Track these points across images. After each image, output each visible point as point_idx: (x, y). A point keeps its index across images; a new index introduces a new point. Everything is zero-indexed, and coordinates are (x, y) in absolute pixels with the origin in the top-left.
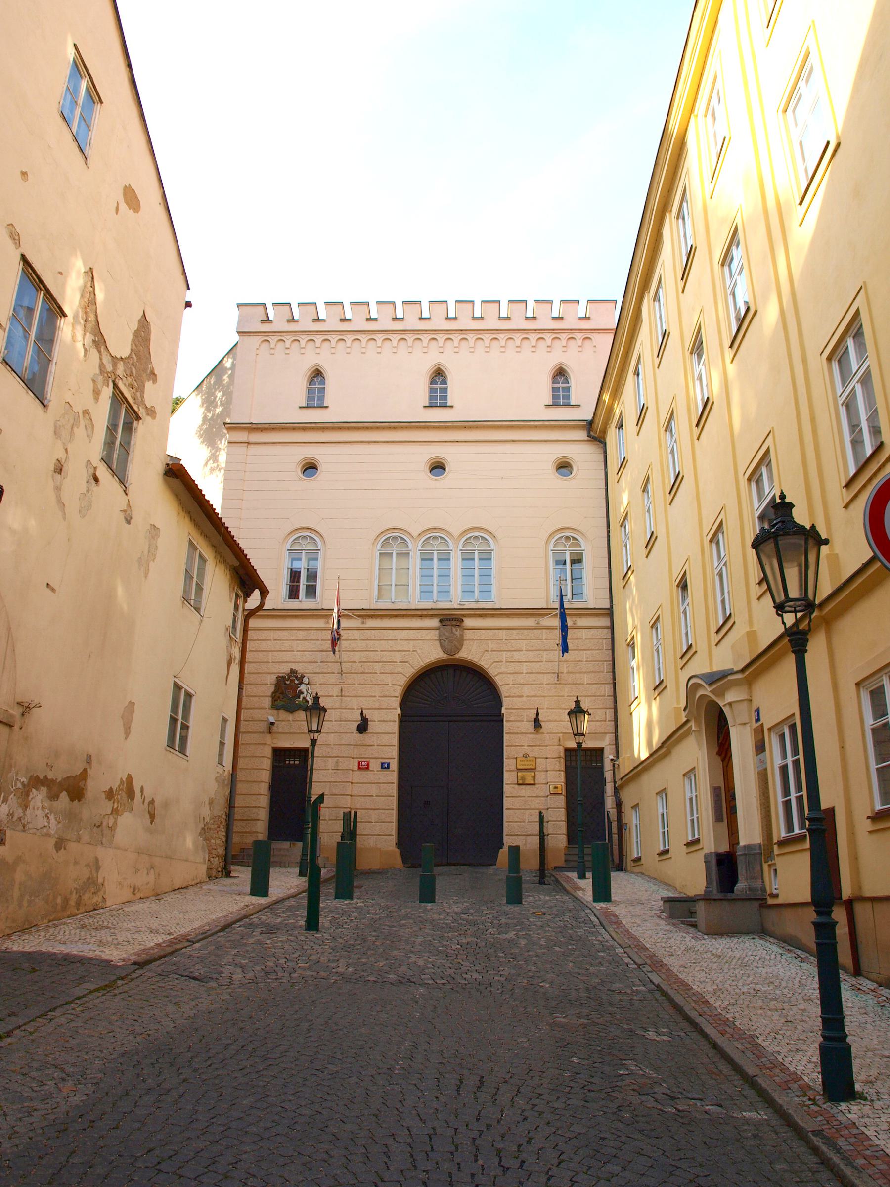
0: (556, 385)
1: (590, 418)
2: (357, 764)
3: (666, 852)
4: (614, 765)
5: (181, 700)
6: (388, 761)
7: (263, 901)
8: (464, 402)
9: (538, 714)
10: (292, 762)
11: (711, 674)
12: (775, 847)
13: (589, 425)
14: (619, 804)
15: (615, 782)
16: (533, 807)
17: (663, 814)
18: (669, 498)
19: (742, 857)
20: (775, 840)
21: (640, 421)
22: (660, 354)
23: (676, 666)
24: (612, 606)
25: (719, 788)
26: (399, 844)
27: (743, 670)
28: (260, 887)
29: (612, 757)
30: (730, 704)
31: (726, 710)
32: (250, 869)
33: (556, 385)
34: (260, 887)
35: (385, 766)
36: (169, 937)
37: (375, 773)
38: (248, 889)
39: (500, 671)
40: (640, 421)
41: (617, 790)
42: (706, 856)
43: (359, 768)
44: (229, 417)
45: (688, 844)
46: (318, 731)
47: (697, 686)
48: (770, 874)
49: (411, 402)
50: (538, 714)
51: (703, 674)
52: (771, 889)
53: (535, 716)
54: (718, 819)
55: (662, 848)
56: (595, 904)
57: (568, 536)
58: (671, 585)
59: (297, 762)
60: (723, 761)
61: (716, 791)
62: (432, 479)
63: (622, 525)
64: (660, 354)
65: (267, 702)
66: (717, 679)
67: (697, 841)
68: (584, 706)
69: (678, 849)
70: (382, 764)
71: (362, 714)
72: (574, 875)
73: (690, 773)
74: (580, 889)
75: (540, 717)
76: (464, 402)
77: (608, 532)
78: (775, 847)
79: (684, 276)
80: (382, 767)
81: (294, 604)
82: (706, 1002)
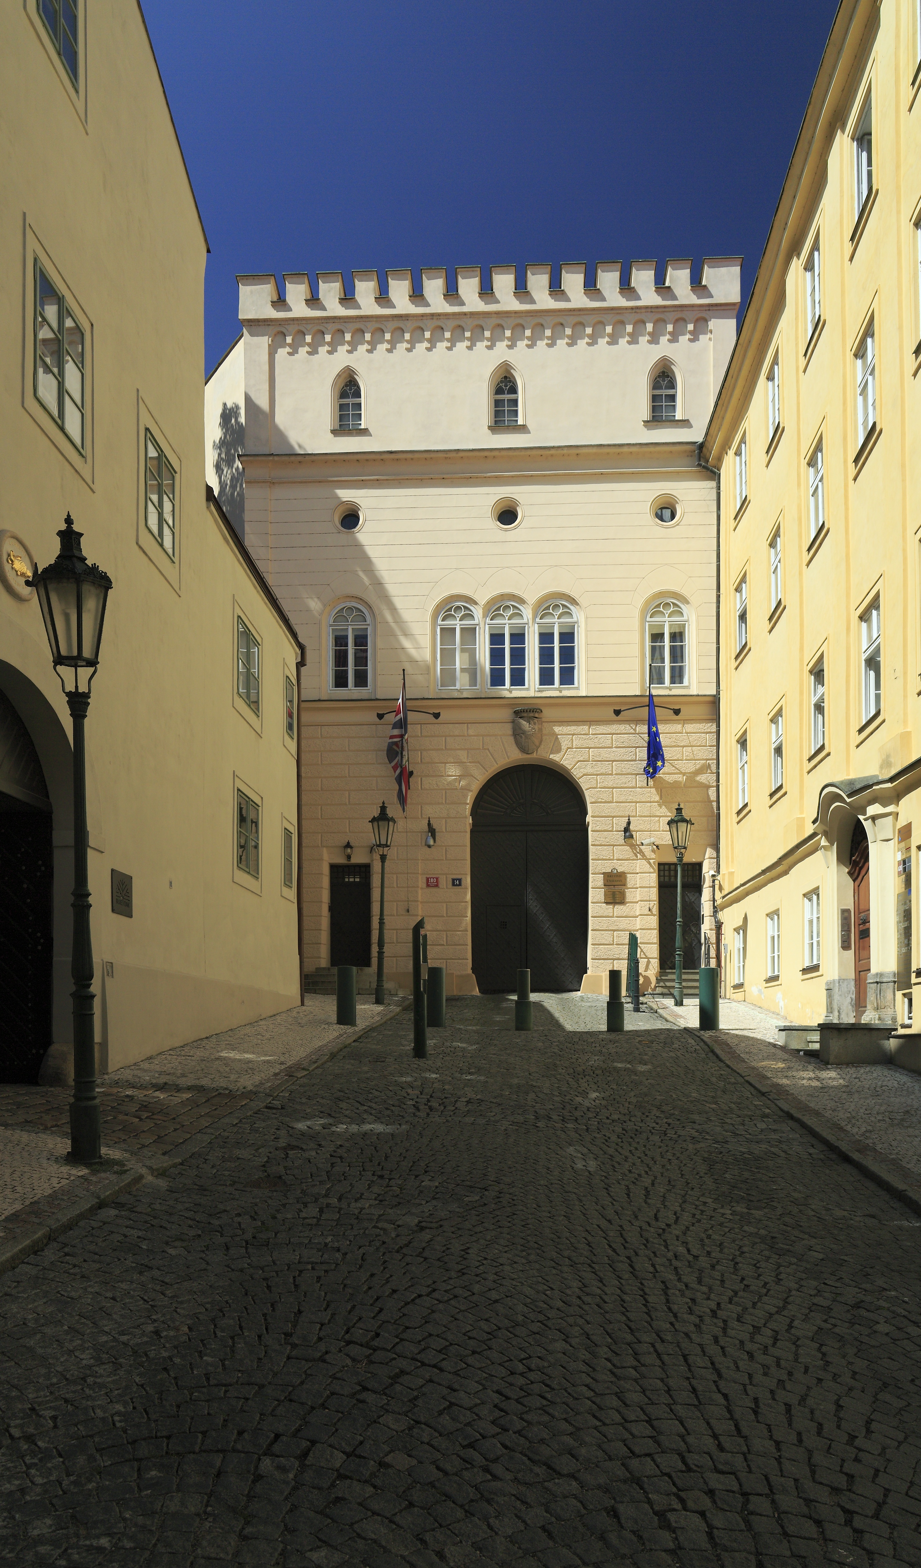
0: (657, 392)
1: (846, 1478)
2: (425, 881)
3: (775, 978)
4: (714, 881)
5: (247, 817)
6: (459, 877)
7: (349, 1029)
8: (544, 421)
9: (629, 823)
10: (351, 880)
11: (851, 782)
12: (913, 975)
13: (701, 448)
14: (719, 926)
15: (714, 900)
16: (622, 927)
17: (773, 938)
18: (806, 557)
19: (872, 985)
20: (914, 968)
21: (772, 447)
22: (808, 353)
23: (801, 769)
24: (718, 692)
25: (848, 911)
26: (473, 969)
27: (892, 780)
28: (346, 1016)
29: (712, 872)
30: (874, 818)
31: (867, 825)
32: (335, 997)
33: (657, 392)
34: (346, 1016)
35: (457, 883)
36: (283, 1067)
37: (445, 891)
38: (334, 1017)
39: (585, 771)
40: (772, 447)
41: (716, 910)
42: (827, 984)
43: (428, 886)
44: (243, 445)
45: (805, 971)
46: (387, 846)
47: (837, 797)
48: (903, 1003)
49: (471, 430)
50: (629, 823)
51: (842, 782)
52: (903, 1019)
53: (625, 825)
54: (845, 945)
55: (770, 974)
56: (702, 1032)
57: (667, 602)
58: (801, 670)
59: (357, 880)
60: (854, 881)
61: (845, 914)
62: (501, 529)
63: (738, 589)
64: (808, 353)
65: (631, 880)
66: (861, 790)
67: (816, 968)
68: (686, 814)
69: (790, 973)
70: (453, 880)
71: (429, 824)
72: (670, 1002)
73: (813, 894)
74: (681, 1017)
75: (631, 827)
76: (544, 421)
77: (718, 597)
78: (913, 975)
79: (856, 236)
80: (453, 885)
81: (341, 693)
82: (841, 1129)
